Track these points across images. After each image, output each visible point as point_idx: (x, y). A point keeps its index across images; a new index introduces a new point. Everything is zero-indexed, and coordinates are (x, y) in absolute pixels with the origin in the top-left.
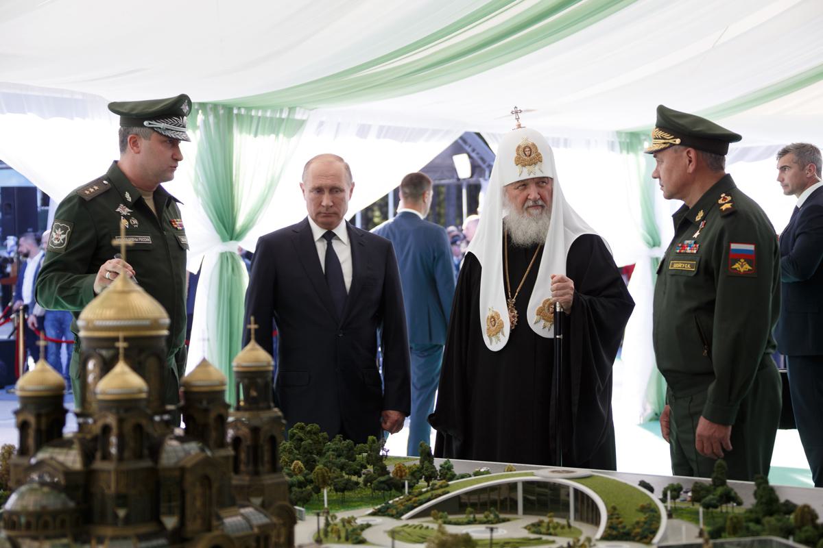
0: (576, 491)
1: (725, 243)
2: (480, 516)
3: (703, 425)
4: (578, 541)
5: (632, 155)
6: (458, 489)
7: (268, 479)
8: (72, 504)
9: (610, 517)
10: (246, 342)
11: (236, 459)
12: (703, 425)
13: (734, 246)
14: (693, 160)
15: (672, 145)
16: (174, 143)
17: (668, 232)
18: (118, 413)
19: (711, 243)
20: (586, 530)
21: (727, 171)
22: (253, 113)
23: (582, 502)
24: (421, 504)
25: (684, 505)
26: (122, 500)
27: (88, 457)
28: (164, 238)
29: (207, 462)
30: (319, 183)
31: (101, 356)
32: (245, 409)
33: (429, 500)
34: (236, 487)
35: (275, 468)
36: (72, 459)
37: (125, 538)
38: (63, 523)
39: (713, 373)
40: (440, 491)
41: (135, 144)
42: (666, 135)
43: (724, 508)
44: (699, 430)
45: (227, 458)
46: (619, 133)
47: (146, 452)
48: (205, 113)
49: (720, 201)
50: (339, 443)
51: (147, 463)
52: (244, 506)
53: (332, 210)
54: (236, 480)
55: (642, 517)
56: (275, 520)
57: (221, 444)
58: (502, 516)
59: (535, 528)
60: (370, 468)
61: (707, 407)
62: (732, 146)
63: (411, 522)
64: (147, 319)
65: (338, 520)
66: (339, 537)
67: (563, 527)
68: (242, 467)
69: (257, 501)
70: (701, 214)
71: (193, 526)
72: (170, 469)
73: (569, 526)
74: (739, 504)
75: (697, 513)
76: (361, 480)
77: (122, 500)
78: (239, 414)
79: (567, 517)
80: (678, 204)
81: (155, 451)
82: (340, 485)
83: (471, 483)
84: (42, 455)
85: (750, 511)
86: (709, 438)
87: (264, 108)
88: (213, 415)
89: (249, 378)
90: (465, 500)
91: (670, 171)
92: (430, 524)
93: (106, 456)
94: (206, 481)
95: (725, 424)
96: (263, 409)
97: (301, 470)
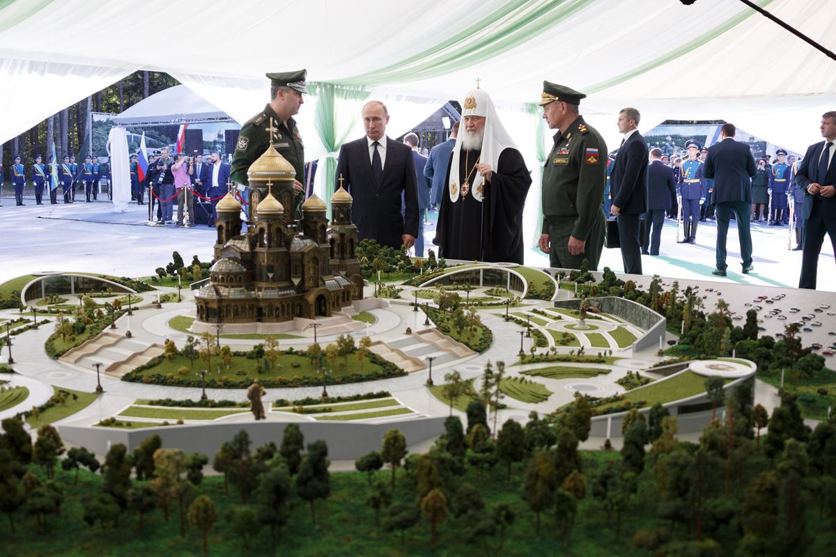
0: (511, 274)
1: (584, 147)
2: (460, 286)
3: (572, 241)
4: (513, 299)
5: (532, 115)
6: (448, 272)
7: (349, 262)
8: (245, 270)
9: (529, 287)
10: (337, 188)
11: (332, 249)
12: (572, 241)
13: (588, 150)
14: (565, 108)
15: (554, 101)
16: (299, 94)
17: (550, 144)
18: (268, 221)
19: (576, 148)
20: (516, 294)
21: (580, 114)
22: (344, 88)
23: (514, 280)
24: (429, 280)
25: (565, 282)
26: (270, 269)
27: (253, 245)
28: (294, 144)
29: (316, 250)
30: (367, 116)
31: (259, 190)
32: (337, 224)
33: (434, 278)
34: (332, 265)
35: (353, 256)
36: (244, 246)
37: (273, 289)
38: (240, 278)
39: (578, 215)
40: (439, 273)
41: (281, 95)
42: (550, 96)
43: (586, 283)
44: (570, 243)
45: (327, 248)
46: (526, 104)
47: (283, 243)
48: (321, 88)
49: (580, 128)
50: (385, 249)
51: (284, 250)
52: (336, 276)
53: (375, 130)
54: (332, 262)
55: (546, 287)
56: (352, 283)
57: (324, 241)
58: (471, 286)
59: (489, 292)
60: (402, 262)
61: (574, 231)
62: (582, 101)
63: (424, 289)
64: (284, 171)
65: (385, 287)
66: (386, 295)
67: (504, 292)
68: (335, 255)
69: (344, 273)
70: (569, 135)
71: (309, 284)
72: (297, 253)
73: (508, 292)
74: (594, 281)
75: (574, 286)
76: (397, 267)
77: (270, 269)
78: (334, 226)
79: (506, 288)
80: (556, 131)
81: (288, 243)
82: (387, 269)
83: (455, 270)
84: (228, 244)
85: (601, 284)
86: (575, 247)
87: (350, 86)
88: (319, 225)
89: (339, 208)
90: (452, 278)
91: (553, 114)
92: (436, 291)
93: (262, 245)
94: (315, 260)
95: (583, 240)
96: (346, 224)
97: (366, 262)
